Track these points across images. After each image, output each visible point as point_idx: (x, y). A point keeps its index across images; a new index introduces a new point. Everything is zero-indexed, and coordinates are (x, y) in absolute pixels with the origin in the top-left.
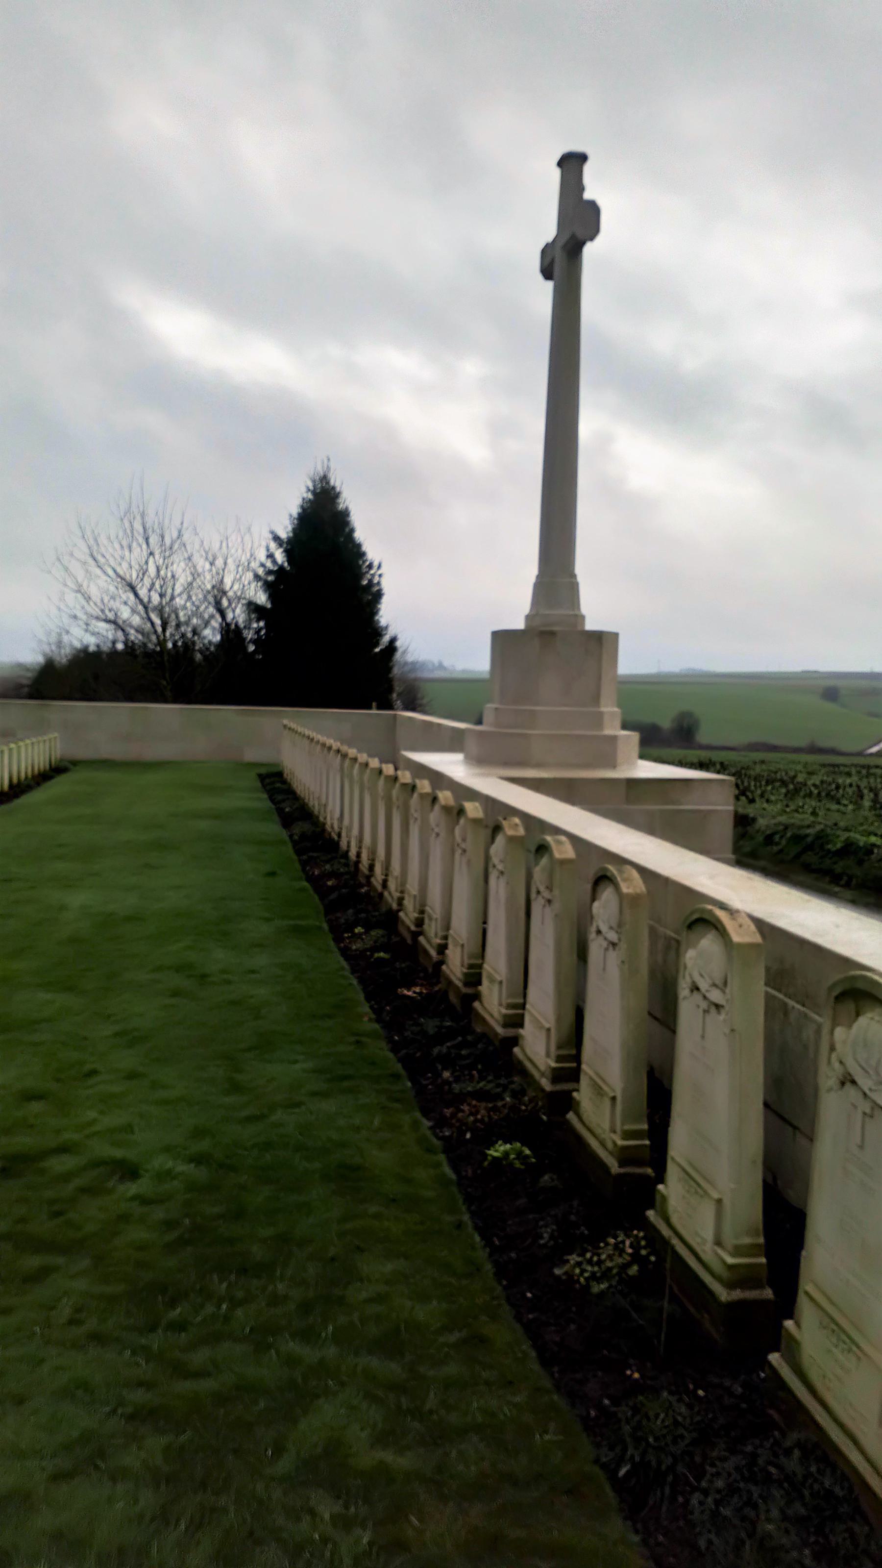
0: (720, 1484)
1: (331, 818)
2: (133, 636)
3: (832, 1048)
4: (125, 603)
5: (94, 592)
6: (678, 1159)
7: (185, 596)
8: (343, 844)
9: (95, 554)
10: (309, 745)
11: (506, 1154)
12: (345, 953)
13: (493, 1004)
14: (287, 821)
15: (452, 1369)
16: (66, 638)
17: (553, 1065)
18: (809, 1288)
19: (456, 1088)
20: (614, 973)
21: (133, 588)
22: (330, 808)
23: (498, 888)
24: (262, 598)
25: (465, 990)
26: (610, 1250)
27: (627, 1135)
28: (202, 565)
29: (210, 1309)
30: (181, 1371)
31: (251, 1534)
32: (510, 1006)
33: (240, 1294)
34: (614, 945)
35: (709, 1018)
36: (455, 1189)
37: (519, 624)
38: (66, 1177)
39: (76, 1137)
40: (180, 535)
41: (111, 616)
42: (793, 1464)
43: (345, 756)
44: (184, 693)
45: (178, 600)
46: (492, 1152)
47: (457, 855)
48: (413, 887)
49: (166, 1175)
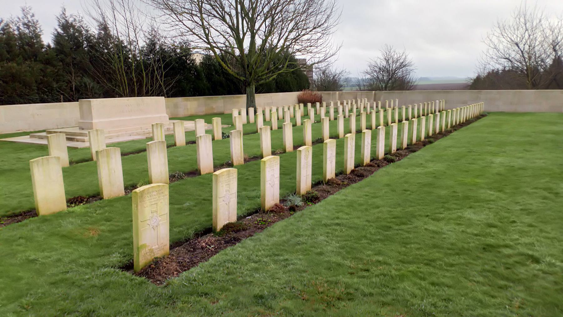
2: (517, 64)
4: (514, 51)
5: (501, 47)
7: (540, 46)
9: (503, 33)
16: (488, 66)
21: (517, 44)
28: (548, 32)
38: (509, 256)
39: (511, 243)
40: (540, 21)
41: (507, 56)
44: (535, 86)
49: (550, 264)
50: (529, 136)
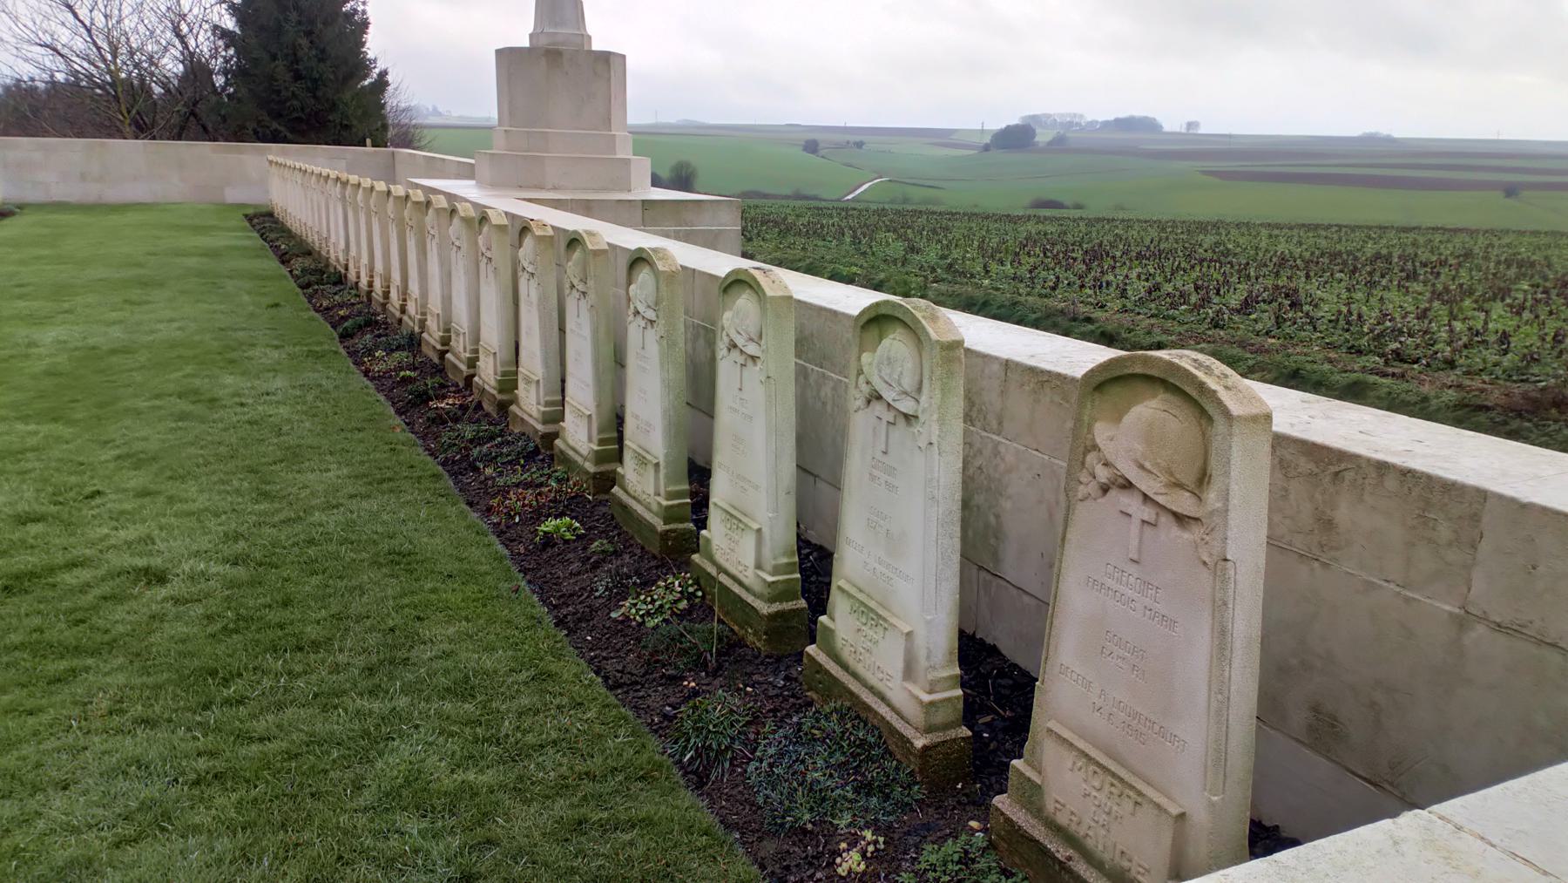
0: (771, 751)
1: (335, 252)
2: (80, 65)
3: (860, 372)
6: (720, 504)
8: (352, 276)
10: (299, 183)
11: (557, 527)
12: (366, 373)
13: (530, 403)
14: (284, 259)
15: (525, 701)
17: (596, 448)
18: (842, 583)
19: (501, 481)
20: (653, 349)
22: (333, 240)
23: (530, 292)
24: (229, 23)
25: (499, 397)
26: (661, 591)
27: (670, 496)
29: (267, 682)
30: (245, 737)
31: (340, 858)
32: (547, 404)
33: (298, 668)
34: (652, 322)
35: (746, 372)
36: (508, 562)
37: (525, 43)
38: (85, 588)
41: (48, 39)
42: (833, 725)
43: (345, 184)
44: (143, 128)
45: (126, 22)
46: (543, 528)
47: (483, 265)
48: (435, 305)
50: (139, 265)
